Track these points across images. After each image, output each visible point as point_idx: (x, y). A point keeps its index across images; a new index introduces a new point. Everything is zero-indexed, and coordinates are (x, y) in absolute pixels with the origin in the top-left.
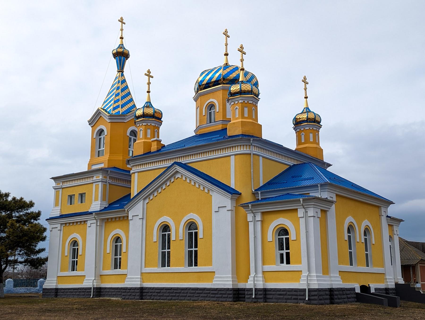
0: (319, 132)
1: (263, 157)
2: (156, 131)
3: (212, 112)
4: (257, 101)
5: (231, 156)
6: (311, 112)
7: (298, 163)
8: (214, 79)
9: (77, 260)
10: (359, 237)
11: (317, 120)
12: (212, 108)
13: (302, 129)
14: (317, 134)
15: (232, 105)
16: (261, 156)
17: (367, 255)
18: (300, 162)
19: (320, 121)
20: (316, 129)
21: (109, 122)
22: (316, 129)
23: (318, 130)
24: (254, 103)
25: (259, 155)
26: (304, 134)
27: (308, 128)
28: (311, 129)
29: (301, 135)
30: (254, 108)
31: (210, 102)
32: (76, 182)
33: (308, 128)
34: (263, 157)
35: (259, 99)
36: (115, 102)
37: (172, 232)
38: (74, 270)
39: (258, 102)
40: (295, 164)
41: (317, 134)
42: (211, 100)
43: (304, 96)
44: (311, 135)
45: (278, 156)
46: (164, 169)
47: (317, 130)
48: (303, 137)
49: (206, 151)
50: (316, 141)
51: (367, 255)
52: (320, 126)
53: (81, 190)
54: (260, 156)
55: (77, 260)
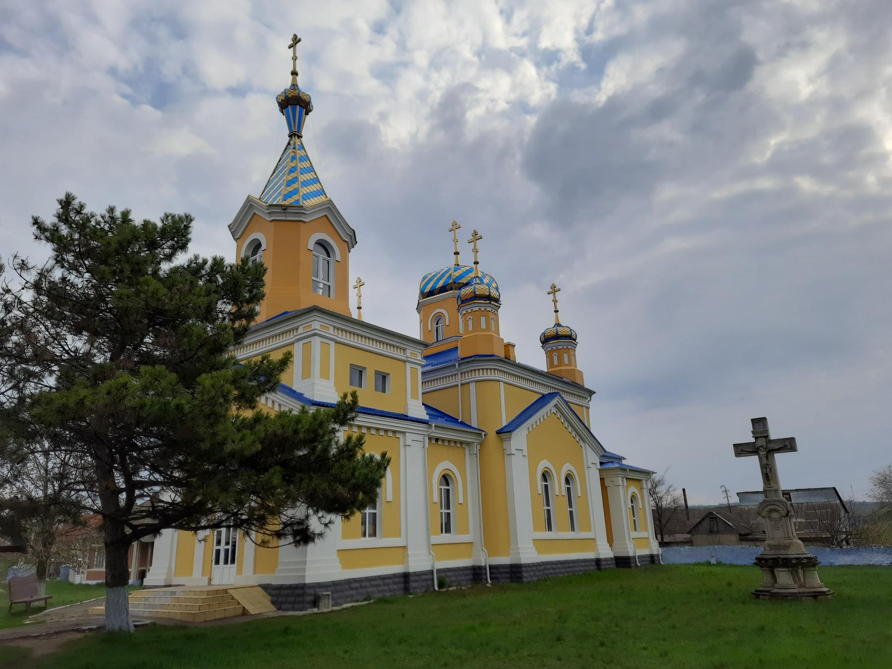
1: (505, 383)
4: (358, 383)
8: (440, 284)
10: (558, 487)
13: (554, 348)
17: (571, 512)
21: (271, 221)
25: (499, 381)
27: (561, 347)
33: (477, 309)
34: (505, 383)
36: (289, 183)
37: (438, 487)
40: (550, 392)
43: (554, 309)
44: (483, 319)
46: (586, 425)
48: (470, 322)
49: (434, 378)
50: (572, 360)
51: (571, 512)
52: (499, 305)
53: (384, 366)
54: (407, 363)
55: (441, 511)
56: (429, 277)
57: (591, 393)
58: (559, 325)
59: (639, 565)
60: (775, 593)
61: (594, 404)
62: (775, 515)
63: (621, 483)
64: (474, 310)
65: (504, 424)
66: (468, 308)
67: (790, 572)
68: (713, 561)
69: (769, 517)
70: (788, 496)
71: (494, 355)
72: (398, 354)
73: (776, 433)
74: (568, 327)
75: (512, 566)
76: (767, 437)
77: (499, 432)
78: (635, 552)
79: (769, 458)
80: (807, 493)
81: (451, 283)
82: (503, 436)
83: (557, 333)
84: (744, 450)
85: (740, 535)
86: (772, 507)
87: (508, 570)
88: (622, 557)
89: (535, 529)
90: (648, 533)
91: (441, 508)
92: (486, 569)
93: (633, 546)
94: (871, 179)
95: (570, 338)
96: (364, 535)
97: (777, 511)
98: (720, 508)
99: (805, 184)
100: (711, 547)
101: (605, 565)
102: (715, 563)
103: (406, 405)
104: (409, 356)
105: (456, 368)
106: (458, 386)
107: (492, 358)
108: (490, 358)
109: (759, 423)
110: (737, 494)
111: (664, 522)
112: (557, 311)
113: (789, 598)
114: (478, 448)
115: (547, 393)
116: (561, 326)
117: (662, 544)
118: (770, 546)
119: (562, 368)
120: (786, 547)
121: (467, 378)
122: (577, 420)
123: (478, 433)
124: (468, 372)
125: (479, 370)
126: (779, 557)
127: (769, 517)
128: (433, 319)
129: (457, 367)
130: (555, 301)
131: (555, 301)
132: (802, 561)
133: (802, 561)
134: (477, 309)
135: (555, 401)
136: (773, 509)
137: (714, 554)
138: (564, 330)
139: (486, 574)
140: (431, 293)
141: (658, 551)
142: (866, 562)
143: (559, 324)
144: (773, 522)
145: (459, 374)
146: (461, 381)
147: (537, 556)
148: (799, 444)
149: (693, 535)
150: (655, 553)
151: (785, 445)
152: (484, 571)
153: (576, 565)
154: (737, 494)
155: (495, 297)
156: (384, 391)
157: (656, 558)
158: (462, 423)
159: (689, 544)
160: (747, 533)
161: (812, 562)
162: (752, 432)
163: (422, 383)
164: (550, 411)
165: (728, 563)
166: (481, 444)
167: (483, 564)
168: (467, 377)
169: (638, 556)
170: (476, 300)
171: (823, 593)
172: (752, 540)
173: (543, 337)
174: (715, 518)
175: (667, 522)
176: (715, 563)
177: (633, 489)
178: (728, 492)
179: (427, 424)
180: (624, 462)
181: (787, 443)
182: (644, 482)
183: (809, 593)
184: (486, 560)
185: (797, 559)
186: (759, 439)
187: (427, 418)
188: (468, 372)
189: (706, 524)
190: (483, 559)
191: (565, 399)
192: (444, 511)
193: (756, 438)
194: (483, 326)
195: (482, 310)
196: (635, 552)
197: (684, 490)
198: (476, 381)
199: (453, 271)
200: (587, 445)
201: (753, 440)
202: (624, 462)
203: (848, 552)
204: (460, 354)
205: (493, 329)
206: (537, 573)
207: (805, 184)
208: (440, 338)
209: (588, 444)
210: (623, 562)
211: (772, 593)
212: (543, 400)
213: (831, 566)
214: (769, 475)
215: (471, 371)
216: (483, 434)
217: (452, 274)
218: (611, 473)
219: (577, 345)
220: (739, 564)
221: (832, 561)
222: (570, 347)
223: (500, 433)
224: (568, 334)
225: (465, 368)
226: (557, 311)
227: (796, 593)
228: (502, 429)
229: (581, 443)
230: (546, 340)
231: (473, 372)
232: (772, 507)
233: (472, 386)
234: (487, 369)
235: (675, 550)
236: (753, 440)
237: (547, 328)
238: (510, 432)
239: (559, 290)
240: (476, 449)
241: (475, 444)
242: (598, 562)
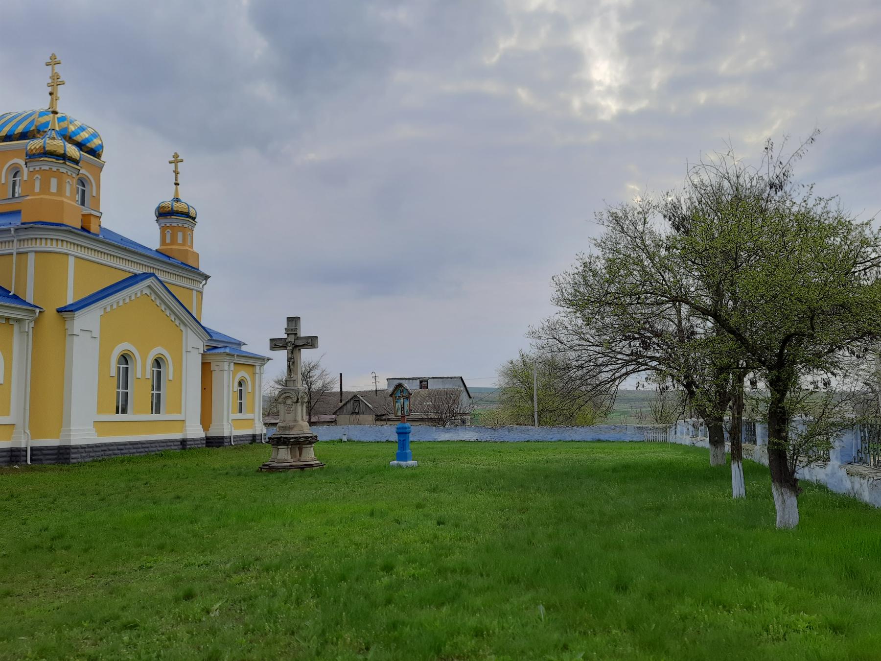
0: (193, 230)
1: (76, 257)
2: (68, 182)
5: (29, 253)
6: (182, 203)
7: (149, 272)
8: (20, 129)
9: (152, 392)
10: (142, 369)
13: (168, 225)
18: (152, 269)
26: (171, 232)
31: (14, 164)
32: (9, 247)
38: (118, 413)
40: (146, 272)
42: (16, 160)
50: (188, 238)
55: (152, 392)
57: (207, 277)
58: (177, 200)
59: (233, 444)
60: (272, 467)
61: (209, 288)
62: (289, 402)
63: (226, 368)
64: (42, 169)
65: (70, 301)
66: (36, 165)
67: (289, 449)
68: (345, 439)
69: (285, 403)
70: (426, 383)
73: (305, 331)
74: (186, 203)
75: (59, 448)
76: (296, 334)
77: (59, 311)
78: (231, 433)
79: (295, 352)
80: (440, 380)
81: (33, 130)
82: (65, 315)
83: (172, 208)
84: (277, 344)
85: (377, 415)
86: (287, 395)
87: (56, 451)
88: (217, 437)
89: (100, 410)
90: (255, 415)
91: (118, 388)
92: (26, 451)
93: (230, 427)
94: (576, 103)
95: (188, 216)
96: (152, 413)
97: (291, 398)
98: (365, 394)
99: (523, 94)
100: (346, 427)
101: (190, 445)
102: (346, 440)
105: (11, 233)
106: (13, 254)
107: (59, 227)
108: (57, 226)
109: (293, 321)
110: (387, 379)
111: (313, 404)
112: (178, 184)
113: (281, 470)
114: (32, 325)
115: (140, 273)
117: (311, 424)
118: (279, 427)
119: (174, 247)
120: (290, 428)
121: (27, 247)
122: (177, 304)
123: (32, 308)
124: (9, 242)
125: (41, 239)
126: (281, 437)
127: (285, 403)
128: (10, 169)
129: (12, 232)
130: (176, 173)
131: (176, 173)
132: (299, 440)
133: (299, 440)
134: (47, 168)
135: (147, 282)
136: (288, 396)
137: (346, 433)
138: (180, 207)
139: (26, 456)
141: (262, 430)
142: (460, 439)
143: (177, 198)
144: (287, 408)
145: (15, 241)
146: (17, 249)
147: (96, 437)
148: (320, 342)
149: (338, 416)
150: (258, 432)
151: (307, 342)
152: (24, 453)
153: (152, 445)
154: (387, 379)
157: (257, 438)
158: (15, 297)
159: (333, 424)
160: (384, 413)
161: (309, 441)
162: (285, 329)
164: (142, 291)
165: (356, 440)
166: (36, 321)
167: (23, 446)
168: (26, 246)
169: (233, 436)
170: (46, 157)
171: (311, 466)
172: (384, 420)
173: (157, 213)
174: (359, 401)
175: (315, 404)
176: (346, 440)
177: (242, 373)
178: (377, 377)
180: (244, 348)
181: (310, 341)
182: (258, 368)
183: (301, 465)
184: (27, 442)
185: (295, 438)
186: (290, 335)
188: (5, 242)
189: (350, 406)
190: (23, 440)
191: (159, 278)
192: (155, 392)
193: (288, 334)
195: (36, 170)
196: (231, 433)
197: (341, 374)
198: (36, 252)
199: (37, 116)
200: (189, 329)
201: (285, 336)
202: (244, 348)
203: (448, 431)
204: (25, 217)
205: (68, 194)
206: (92, 454)
207: (523, 94)
208: (17, 195)
209: (190, 328)
210: (213, 442)
211: (269, 467)
212: (134, 279)
213: (434, 441)
214: (292, 367)
215: (5, 242)
216: (38, 311)
217: (36, 119)
218: (215, 358)
219: (195, 224)
220: (365, 441)
221: (436, 437)
222: (186, 226)
223: (61, 312)
224: (185, 211)
225: (23, 235)
226: (178, 184)
227: (287, 466)
228: (65, 307)
229: (182, 327)
230: (163, 213)
231: (34, 241)
232: (287, 395)
233: (31, 257)
235: (315, 428)
236: (285, 336)
237: (162, 201)
238: (72, 311)
239: (182, 161)
240: (28, 326)
241: (27, 321)
242: (183, 442)
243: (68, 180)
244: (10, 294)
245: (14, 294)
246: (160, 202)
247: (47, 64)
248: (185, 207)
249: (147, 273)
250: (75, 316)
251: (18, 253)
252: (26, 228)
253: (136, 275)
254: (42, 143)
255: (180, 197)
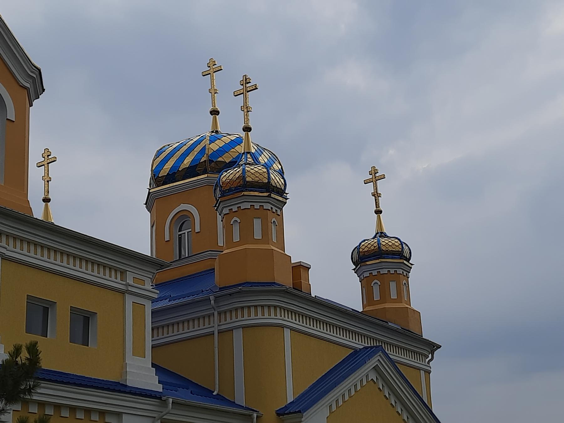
0: (408, 278)
1: (292, 329)
3: (185, 233)
8: (187, 162)
11: (274, 184)
12: (184, 225)
13: (375, 273)
14: (405, 283)
15: (225, 214)
16: (288, 327)
19: (283, 188)
20: (270, 209)
22: (270, 209)
23: (406, 274)
24: (405, 273)
25: (283, 327)
26: (379, 284)
27: (385, 271)
28: (391, 273)
29: (372, 285)
30: (406, 282)
35: (412, 265)
39: (410, 270)
41: (405, 283)
44: (257, 224)
45: (288, 314)
47: (275, 211)
48: (236, 230)
54: (285, 329)
56: (168, 151)
57: (433, 347)
58: (381, 234)
65: (290, 399)
71: (274, 283)
72: (114, 281)
74: (397, 238)
77: (280, 413)
103: (124, 366)
104: (130, 281)
116: (386, 236)
119: (387, 305)
121: (229, 321)
129: (212, 302)
130: (376, 195)
131: (376, 195)
135: (373, 362)
138: (390, 244)
140: (172, 177)
145: (216, 313)
155: (279, 186)
156: (85, 342)
158: (220, 398)
163: (153, 329)
164: (367, 376)
179: (160, 398)
187: (159, 388)
191: (390, 356)
194: (258, 235)
198: (244, 327)
216: (255, 415)
223: (283, 415)
224: (397, 249)
233: (238, 335)
234: (263, 306)
237: (363, 240)
238: (299, 412)
243: (274, 219)
244: (214, 394)
245: (218, 394)
246: (360, 242)
247: (204, 74)
248: (397, 244)
249: (372, 348)
250: (303, 419)
251: (220, 332)
252: (230, 295)
253: (356, 352)
254: (240, 172)
255: (385, 231)
